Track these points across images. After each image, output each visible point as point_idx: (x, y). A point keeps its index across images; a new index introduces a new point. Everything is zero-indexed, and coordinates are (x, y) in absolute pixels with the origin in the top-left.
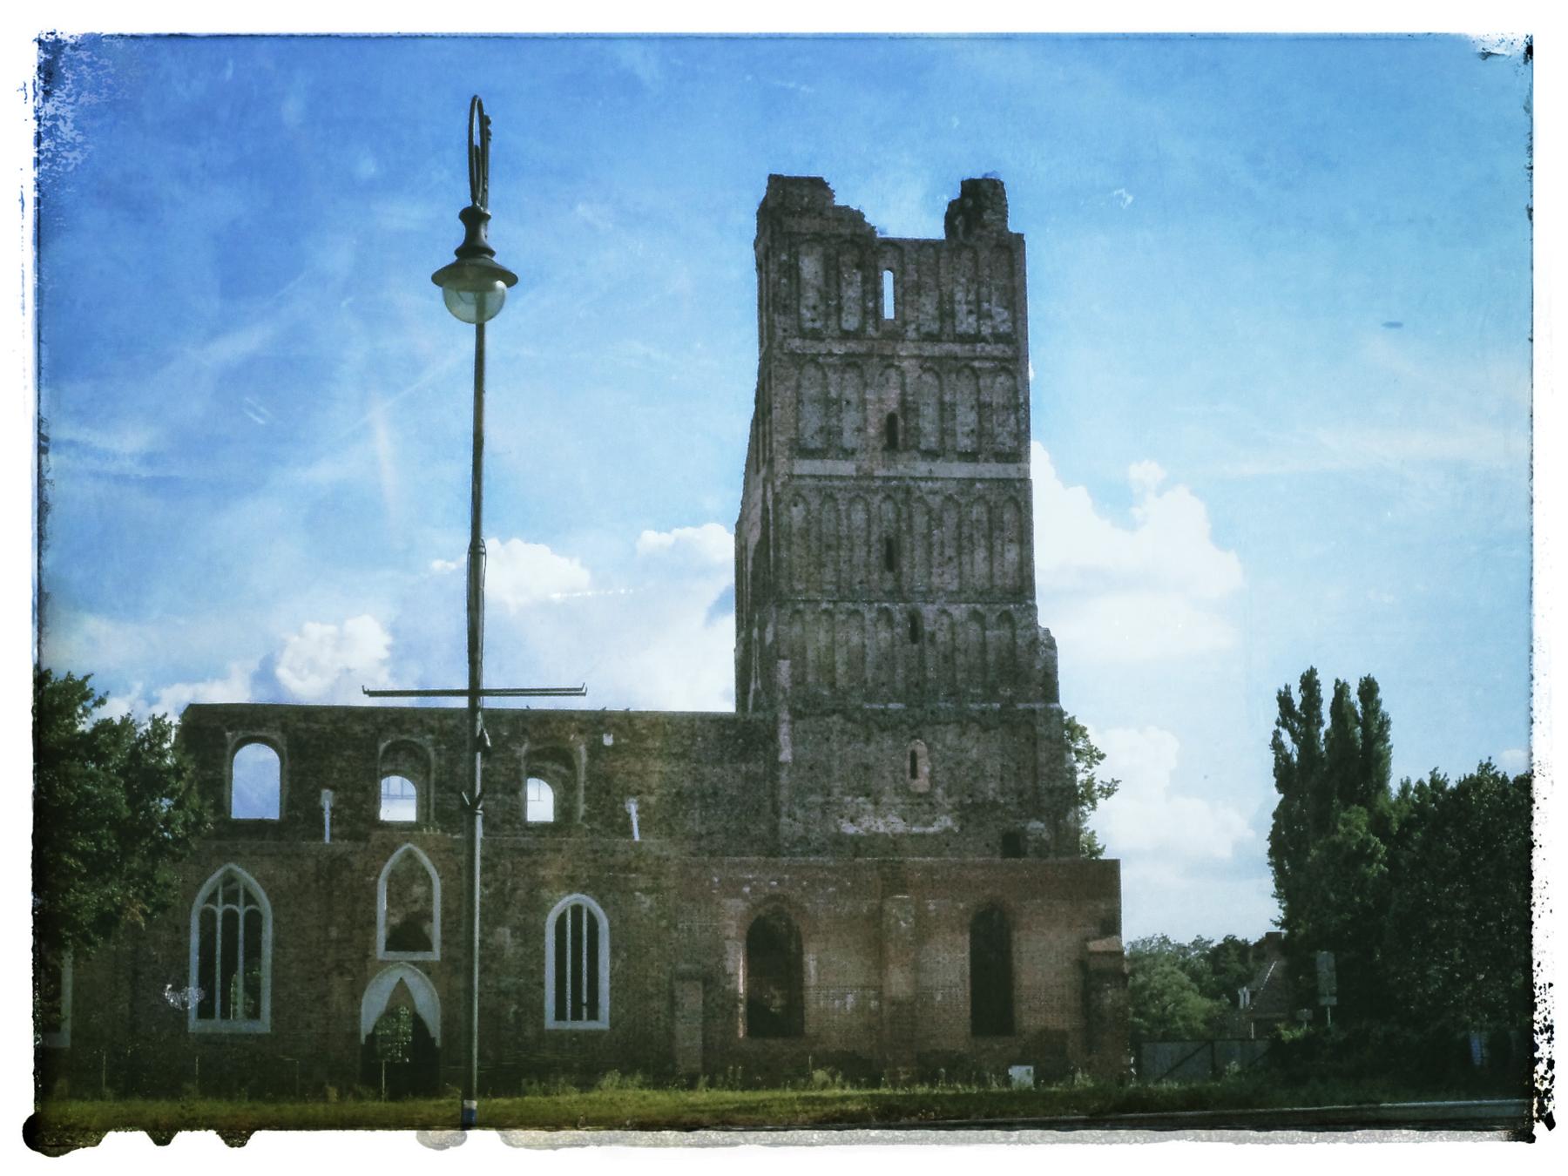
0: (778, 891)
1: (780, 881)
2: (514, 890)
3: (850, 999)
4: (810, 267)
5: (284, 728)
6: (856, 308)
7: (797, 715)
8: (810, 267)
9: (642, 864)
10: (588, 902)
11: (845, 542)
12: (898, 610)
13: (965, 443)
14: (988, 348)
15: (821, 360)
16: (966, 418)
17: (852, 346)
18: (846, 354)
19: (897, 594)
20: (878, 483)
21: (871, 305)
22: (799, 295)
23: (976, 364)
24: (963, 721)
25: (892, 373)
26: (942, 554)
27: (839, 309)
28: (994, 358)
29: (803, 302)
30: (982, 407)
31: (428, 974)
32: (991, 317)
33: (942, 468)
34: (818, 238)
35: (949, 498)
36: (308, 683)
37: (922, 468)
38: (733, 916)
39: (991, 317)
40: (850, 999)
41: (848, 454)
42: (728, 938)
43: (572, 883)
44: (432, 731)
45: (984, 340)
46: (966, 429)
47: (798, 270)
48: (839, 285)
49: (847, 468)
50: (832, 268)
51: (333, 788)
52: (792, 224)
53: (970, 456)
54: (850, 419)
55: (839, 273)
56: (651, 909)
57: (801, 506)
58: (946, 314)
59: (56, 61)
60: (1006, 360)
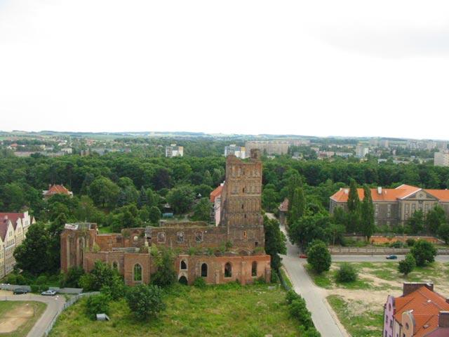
4: (233, 168)
7: (230, 228)
8: (233, 168)
11: (142, 294)
12: (244, 214)
16: (253, 188)
19: (243, 212)
24: (251, 229)
30: (256, 187)
33: (250, 195)
34: (234, 165)
36: (20, 325)
37: (247, 195)
38: (223, 264)
41: (237, 193)
49: (237, 195)
50: (236, 169)
52: (231, 162)
53: (253, 193)
54: (238, 189)
58: (251, 174)
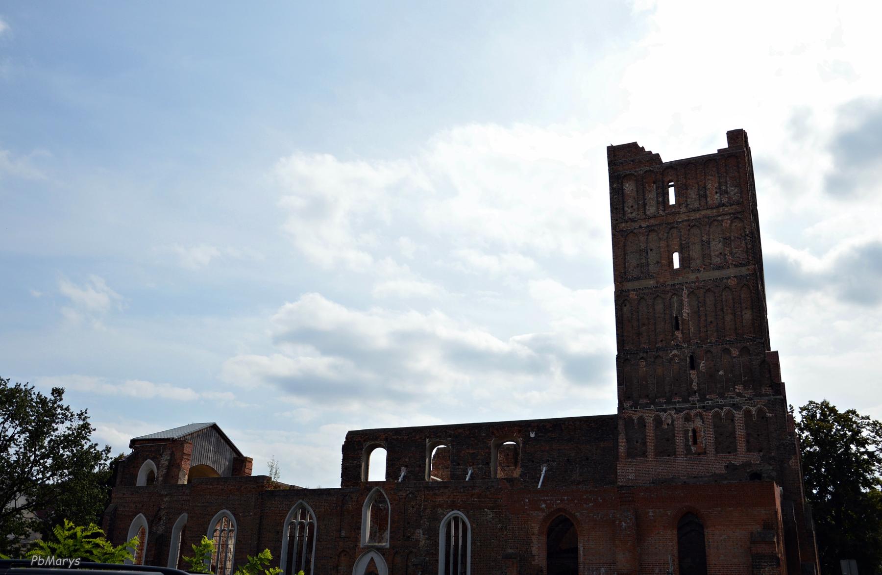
0: (561, 506)
1: (562, 500)
2: (425, 509)
3: (603, 570)
5: (386, 439)
6: (654, 203)
9: (488, 493)
10: (461, 514)
13: (717, 260)
14: (726, 209)
15: (635, 231)
17: (653, 221)
18: (648, 226)
20: (668, 288)
21: (660, 199)
22: (624, 202)
23: (720, 218)
25: (675, 231)
26: (706, 320)
27: (645, 205)
28: (730, 214)
29: (626, 205)
31: (383, 555)
32: (727, 193)
35: (709, 290)
39: (727, 193)
40: (603, 570)
42: (533, 534)
43: (453, 506)
44: (450, 436)
45: (724, 205)
46: (717, 253)
47: (623, 190)
48: (644, 193)
49: (652, 283)
51: (406, 466)
55: (644, 187)
56: (493, 518)
57: (628, 305)
58: (703, 196)
59: (613, 152)
60: (737, 213)
